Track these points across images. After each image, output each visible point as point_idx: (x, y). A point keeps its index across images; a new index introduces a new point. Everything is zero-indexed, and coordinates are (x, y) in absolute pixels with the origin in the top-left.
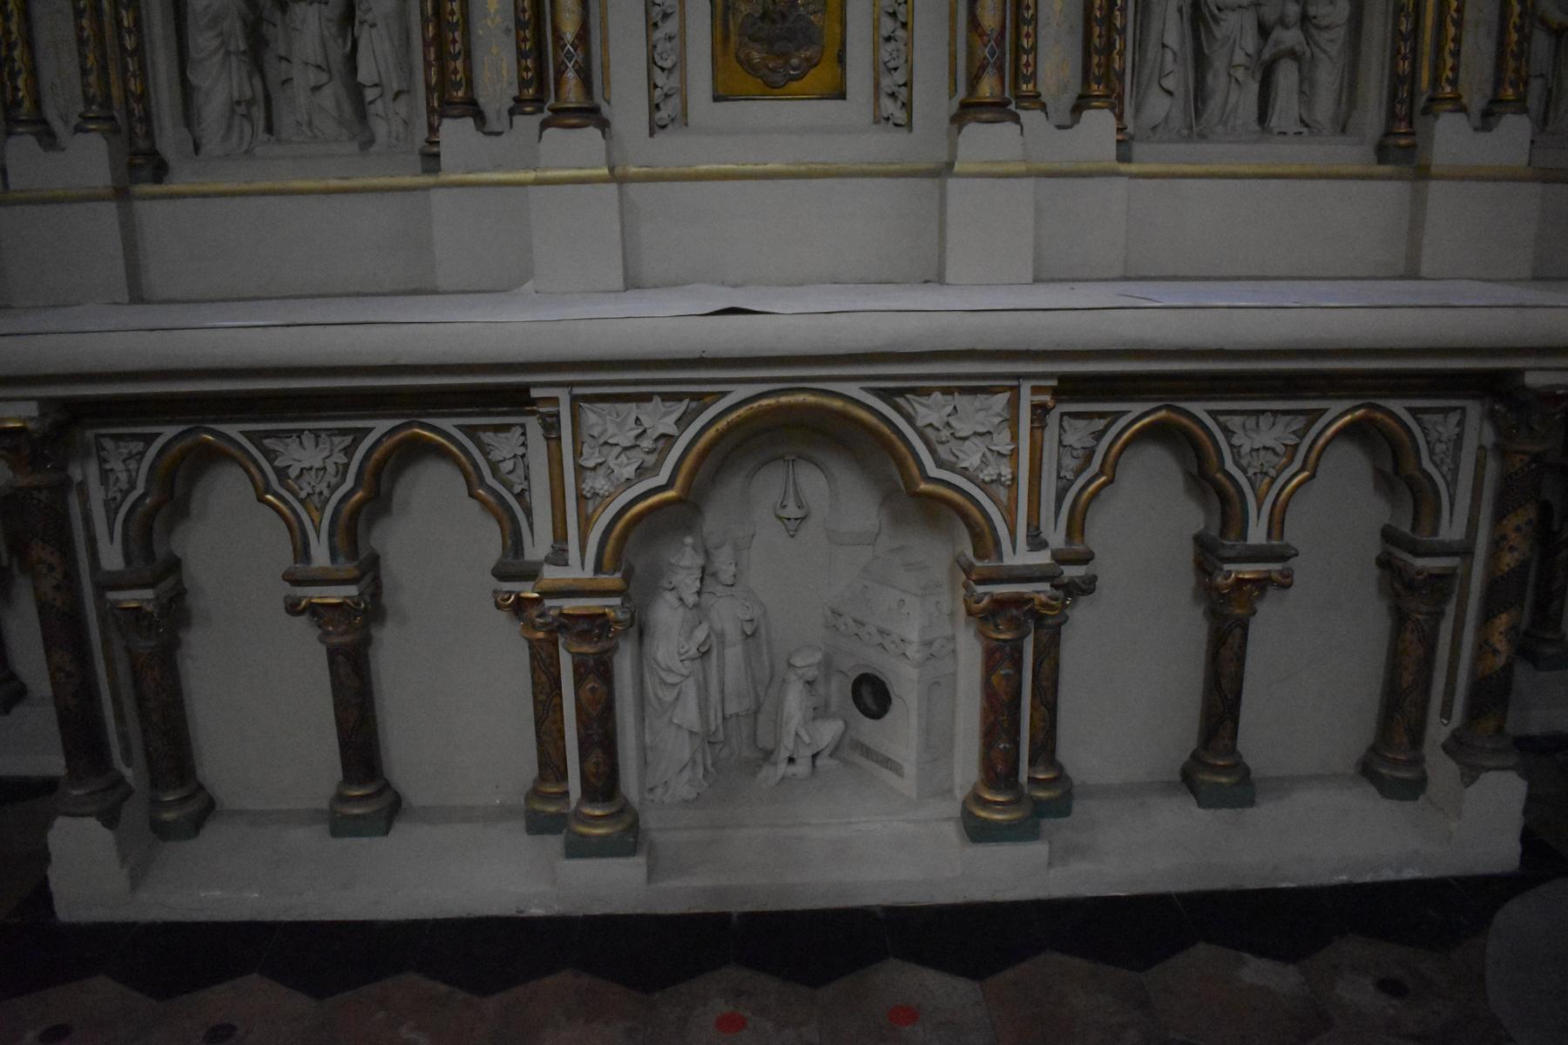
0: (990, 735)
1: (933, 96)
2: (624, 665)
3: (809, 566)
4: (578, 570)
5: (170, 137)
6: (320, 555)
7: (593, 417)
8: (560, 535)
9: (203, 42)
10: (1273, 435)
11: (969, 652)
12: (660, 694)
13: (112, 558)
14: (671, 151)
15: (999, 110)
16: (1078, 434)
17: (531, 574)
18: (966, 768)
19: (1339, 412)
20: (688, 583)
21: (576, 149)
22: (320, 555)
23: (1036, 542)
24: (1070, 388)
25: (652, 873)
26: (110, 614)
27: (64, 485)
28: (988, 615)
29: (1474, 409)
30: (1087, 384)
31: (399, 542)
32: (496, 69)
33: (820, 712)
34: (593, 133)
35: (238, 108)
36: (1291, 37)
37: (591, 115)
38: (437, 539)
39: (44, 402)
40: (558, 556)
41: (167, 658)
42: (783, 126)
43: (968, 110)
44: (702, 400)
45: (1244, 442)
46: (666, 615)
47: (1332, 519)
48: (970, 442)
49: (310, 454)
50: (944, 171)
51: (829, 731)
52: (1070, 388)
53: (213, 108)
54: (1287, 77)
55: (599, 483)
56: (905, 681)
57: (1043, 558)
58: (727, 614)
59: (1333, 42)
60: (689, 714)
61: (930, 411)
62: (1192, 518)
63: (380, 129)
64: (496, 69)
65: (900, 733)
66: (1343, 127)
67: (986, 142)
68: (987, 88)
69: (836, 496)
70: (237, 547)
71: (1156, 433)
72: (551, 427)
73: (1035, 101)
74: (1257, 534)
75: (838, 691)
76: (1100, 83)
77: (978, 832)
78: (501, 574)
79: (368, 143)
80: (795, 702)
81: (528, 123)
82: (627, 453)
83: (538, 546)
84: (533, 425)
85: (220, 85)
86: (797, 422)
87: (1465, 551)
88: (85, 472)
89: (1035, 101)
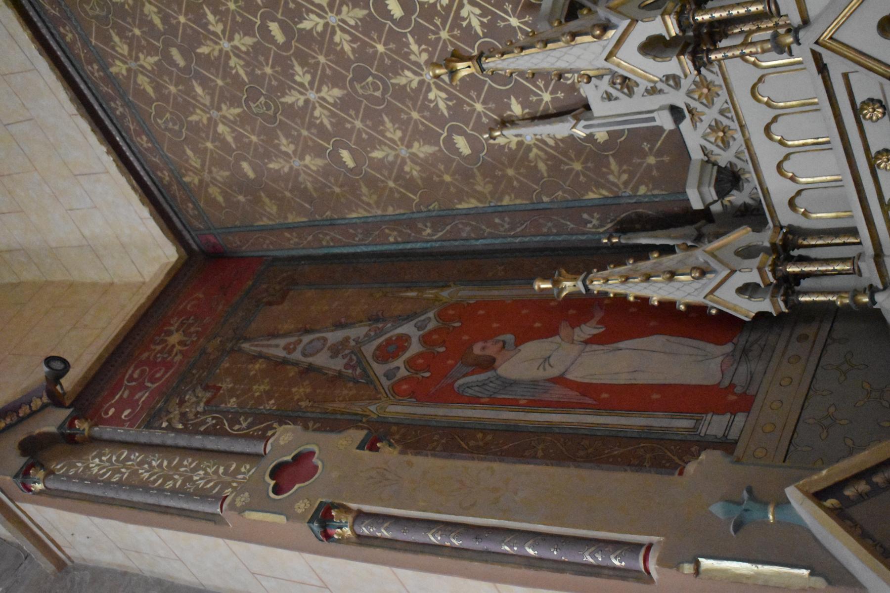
39: (608, 132)
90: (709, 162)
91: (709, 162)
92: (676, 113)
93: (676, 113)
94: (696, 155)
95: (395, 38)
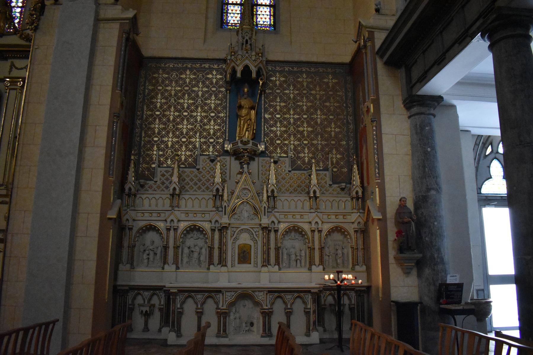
0: (263, 325)
1: (260, 264)
2: (227, 318)
3: (246, 310)
4: (225, 307)
5: (180, 265)
6: (199, 306)
7: (227, 293)
8: (223, 304)
9: (184, 255)
10: (290, 297)
11: (261, 318)
12: (252, 243)
13: (179, 306)
14: (234, 269)
15: (266, 266)
16: (271, 296)
17: (219, 309)
18: (261, 331)
19: (296, 295)
20: (234, 311)
21: (224, 269)
22: (199, 306)
23: (267, 306)
24: (270, 292)
25: (229, 340)
26: (178, 311)
27: (176, 298)
28: (262, 313)
29: (309, 294)
30: (271, 291)
31: (206, 306)
32: (216, 259)
33: (246, 326)
34: (226, 267)
35: (187, 262)
36: (298, 257)
37: (226, 266)
38: (210, 307)
40: (223, 306)
41: (181, 317)
42: (245, 267)
43: (263, 266)
44: (236, 292)
45: (287, 297)
46: (232, 314)
47: (298, 307)
48: (260, 296)
49: (199, 297)
50: (260, 272)
51: (247, 328)
52: (270, 292)
53: (185, 262)
54: (298, 261)
55: (227, 299)
56: (255, 321)
57: (267, 308)
58: (237, 315)
59: (303, 258)
60: (233, 325)
61: (257, 293)
62: (284, 306)
63: (202, 266)
64: (216, 259)
65: (254, 328)
66: (305, 266)
67: (265, 269)
68: (264, 264)
69: (248, 303)
70: (190, 307)
71: (278, 297)
72: (223, 294)
73: (270, 265)
74: (289, 307)
75: (249, 324)
76: (277, 263)
77: (262, 337)
78: (216, 309)
79: (201, 267)
80: (244, 324)
81: (219, 266)
82: (230, 297)
83: (220, 306)
84: (221, 294)
85: (185, 259)
86: (245, 295)
87: (310, 309)
88: (178, 297)
89: (270, 265)
90: (146, 184)
91: (146, 184)
92: (156, 182)
93: (156, 182)
94: (148, 182)
95: (206, 138)
